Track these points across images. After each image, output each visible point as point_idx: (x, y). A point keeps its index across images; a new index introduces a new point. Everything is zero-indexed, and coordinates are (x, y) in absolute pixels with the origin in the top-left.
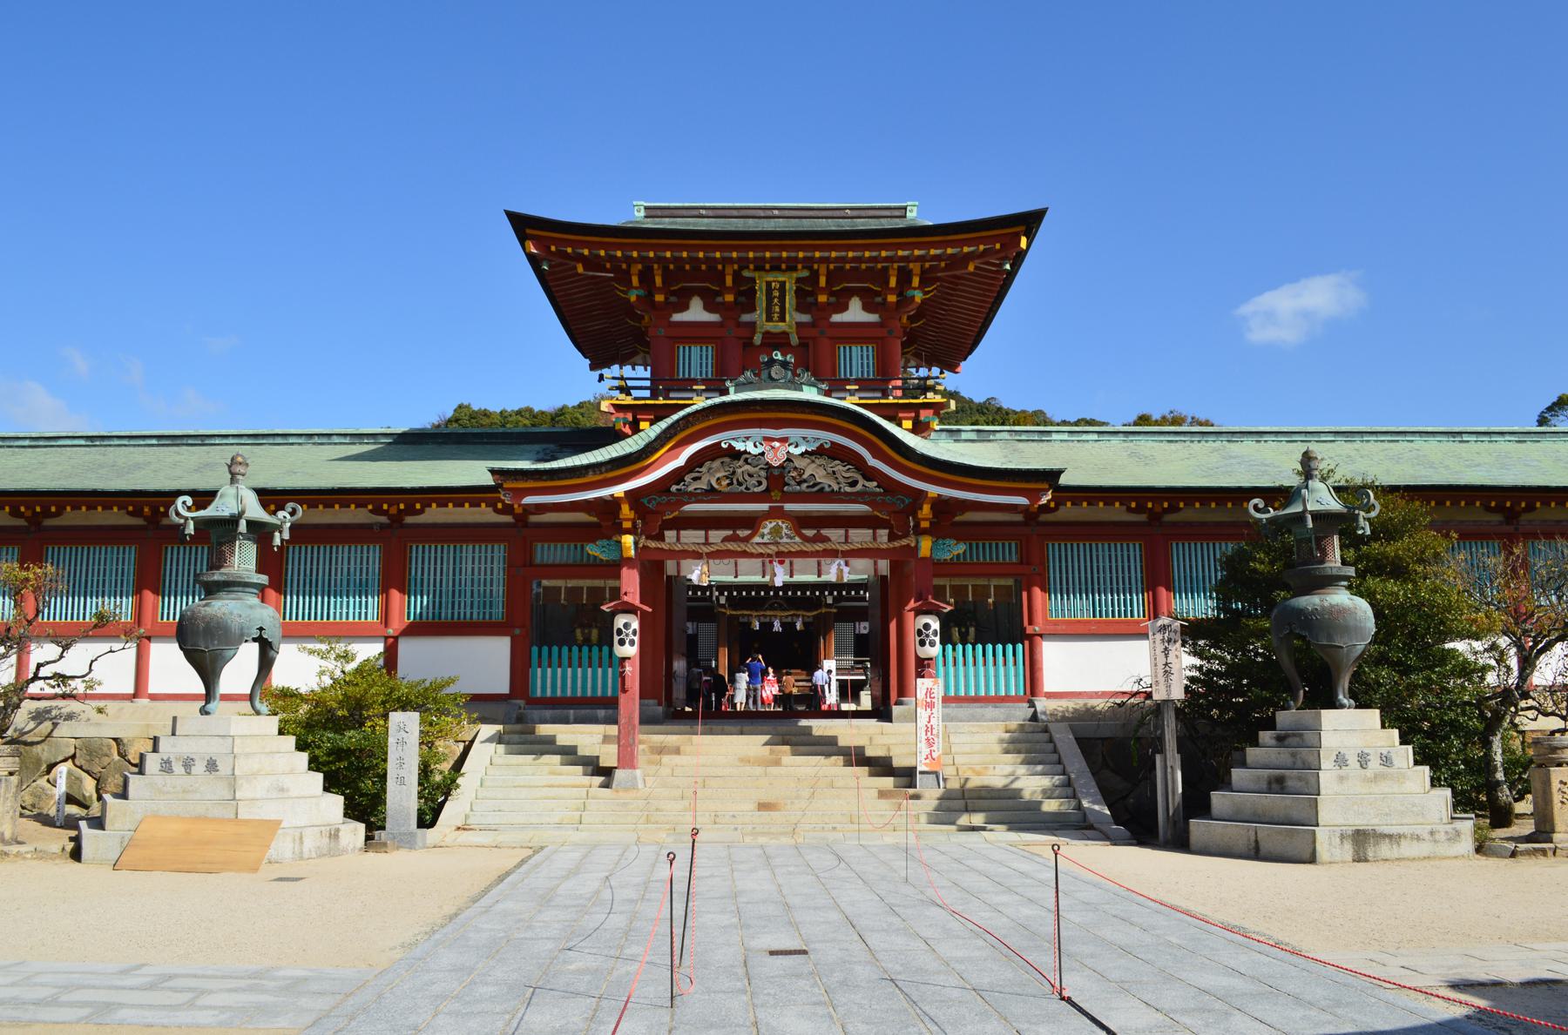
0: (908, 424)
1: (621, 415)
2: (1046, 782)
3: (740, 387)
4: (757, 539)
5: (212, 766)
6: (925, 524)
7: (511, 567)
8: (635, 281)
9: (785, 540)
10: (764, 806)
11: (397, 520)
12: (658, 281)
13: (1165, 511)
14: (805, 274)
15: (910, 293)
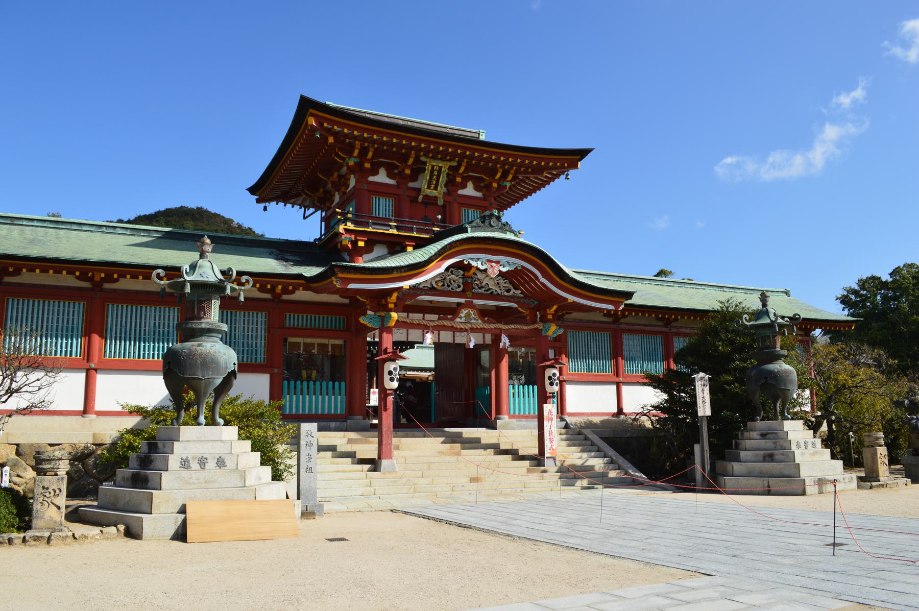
1: (348, 236)
2: (901, 452)
4: (458, 320)
5: (221, 463)
6: (550, 317)
7: (270, 329)
9: (473, 321)
10: (475, 480)
13: (103, 280)
14: (454, 164)
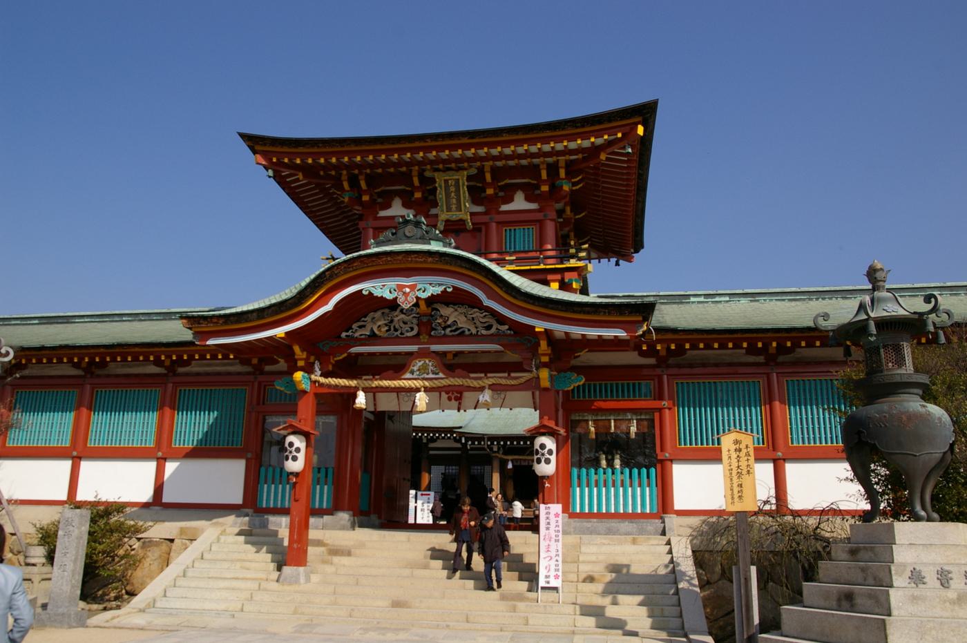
0: (555, 285)
3: (378, 244)
6: (545, 359)
8: (346, 185)
10: (397, 604)
11: (172, 369)
12: (363, 184)
14: (473, 171)
15: (558, 183)
